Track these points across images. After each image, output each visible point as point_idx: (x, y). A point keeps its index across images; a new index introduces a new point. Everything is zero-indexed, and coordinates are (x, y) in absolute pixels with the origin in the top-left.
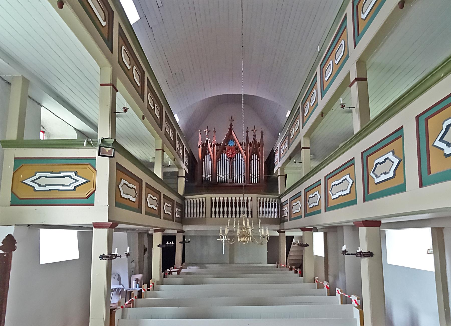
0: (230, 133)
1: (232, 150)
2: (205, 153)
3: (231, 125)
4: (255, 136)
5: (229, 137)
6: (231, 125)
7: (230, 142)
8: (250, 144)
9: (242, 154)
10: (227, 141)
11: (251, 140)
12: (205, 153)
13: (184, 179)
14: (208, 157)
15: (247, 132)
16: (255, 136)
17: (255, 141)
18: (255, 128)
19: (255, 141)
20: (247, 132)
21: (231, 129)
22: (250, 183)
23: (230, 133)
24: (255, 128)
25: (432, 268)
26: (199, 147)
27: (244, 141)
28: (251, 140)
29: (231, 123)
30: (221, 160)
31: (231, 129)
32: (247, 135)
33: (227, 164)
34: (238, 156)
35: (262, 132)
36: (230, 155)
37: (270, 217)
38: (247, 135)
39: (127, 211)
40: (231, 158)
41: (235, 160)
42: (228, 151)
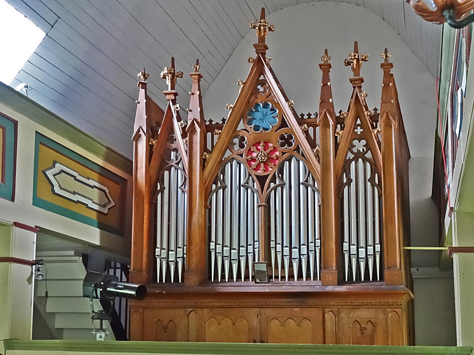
0: (257, 79)
1: (266, 148)
2: (160, 160)
3: (261, 48)
4: (357, 82)
5: (253, 98)
6: (261, 48)
7: (258, 115)
8: (340, 121)
9: (307, 161)
10: (247, 109)
11: (341, 104)
12: (160, 160)
13: (120, 270)
14: (175, 177)
15: (326, 68)
16: (357, 82)
17: (358, 104)
18: (356, 51)
19: (358, 104)
20: (326, 68)
21: (259, 64)
22: (341, 282)
23: (257, 79)
24: (356, 51)
25: (15, 89)
26: (138, 137)
27: (313, 108)
28: (341, 104)
29: (262, 39)
30: (224, 188)
31: (259, 64)
32: (326, 79)
33: (251, 199)
34: (295, 170)
35: (387, 66)
36: (258, 167)
37: (462, 29)
38: (326, 79)
39: (138, 353)
40: (262, 180)
41: (282, 186)
42: (250, 152)
